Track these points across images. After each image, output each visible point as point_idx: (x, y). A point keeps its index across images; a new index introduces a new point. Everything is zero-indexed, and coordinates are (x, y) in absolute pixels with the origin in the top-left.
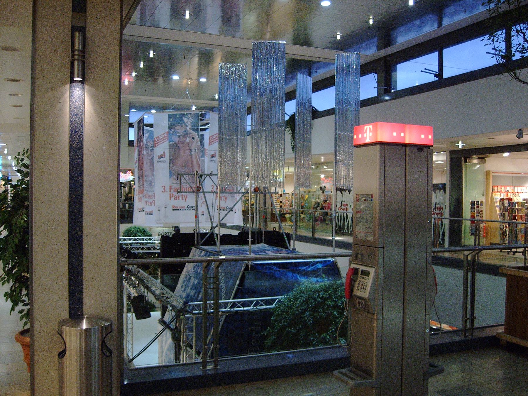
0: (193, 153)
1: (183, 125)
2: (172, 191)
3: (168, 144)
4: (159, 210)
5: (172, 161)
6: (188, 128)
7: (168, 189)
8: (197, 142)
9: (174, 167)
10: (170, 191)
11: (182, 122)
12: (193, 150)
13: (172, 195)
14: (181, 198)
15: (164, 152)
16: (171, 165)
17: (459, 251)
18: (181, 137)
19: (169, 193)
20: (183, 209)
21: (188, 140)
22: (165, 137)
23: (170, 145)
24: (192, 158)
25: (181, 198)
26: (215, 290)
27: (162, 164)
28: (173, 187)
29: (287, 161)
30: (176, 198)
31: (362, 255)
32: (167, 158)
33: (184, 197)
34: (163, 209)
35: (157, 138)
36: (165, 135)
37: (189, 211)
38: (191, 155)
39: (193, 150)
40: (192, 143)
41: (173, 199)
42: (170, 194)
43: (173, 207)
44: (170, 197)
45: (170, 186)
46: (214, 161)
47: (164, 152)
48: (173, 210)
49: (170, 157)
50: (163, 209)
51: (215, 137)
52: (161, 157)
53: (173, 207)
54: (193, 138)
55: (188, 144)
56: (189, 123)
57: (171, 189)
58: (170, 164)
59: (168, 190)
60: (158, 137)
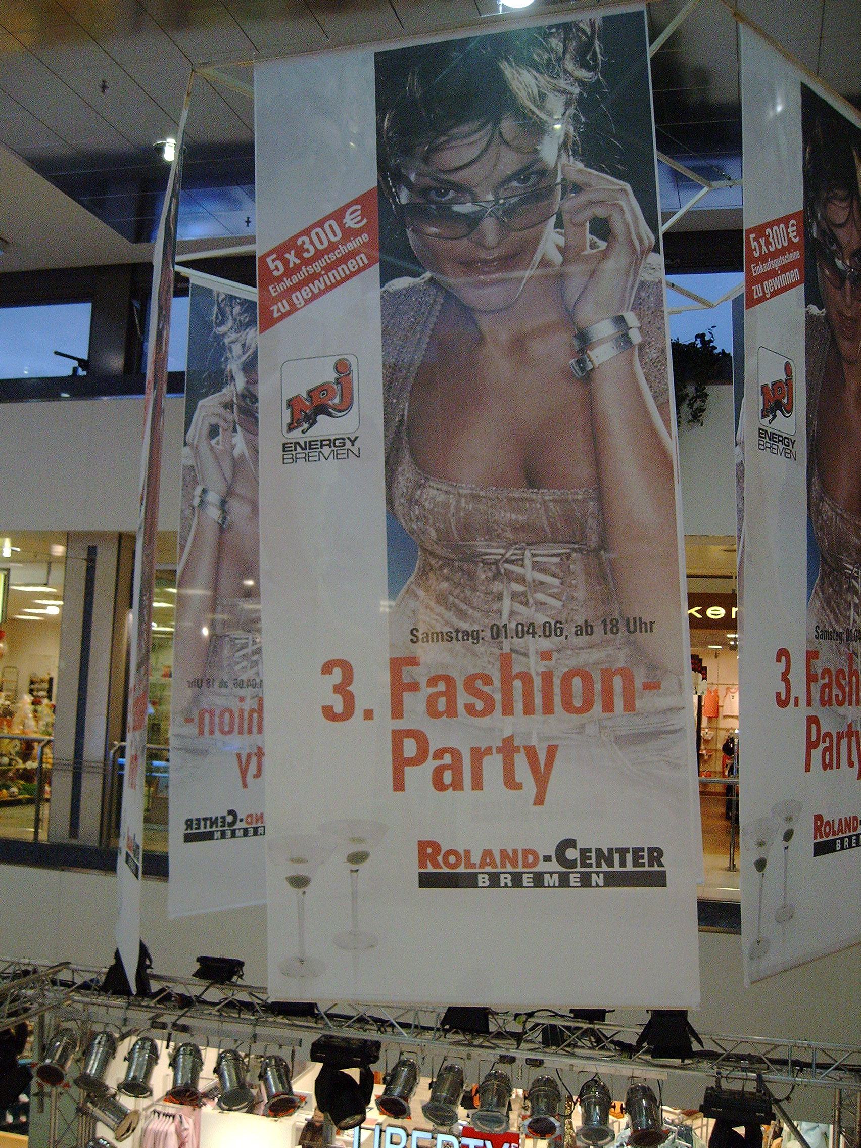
0: (602, 354)
1: (508, 126)
2: (415, 703)
4: (299, 882)
5: (413, 440)
6: (549, 152)
7: (373, 687)
10: (397, 712)
12: (604, 329)
13: (410, 748)
14: (493, 766)
15: (342, 368)
16: (406, 473)
17: (308, 1027)
19: (385, 723)
20: (513, 873)
22: (349, 235)
24: (590, 403)
25: (493, 766)
27: (326, 470)
28: (420, 674)
29: (195, 442)
32: (365, 418)
35: (280, 252)
36: (350, 221)
37: (575, 894)
38: (585, 376)
39: (604, 329)
41: (419, 777)
42: (398, 737)
43: (427, 849)
44: (400, 764)
45: (397, 665)
46: (340, 446)
47: (342, 368)
48: (426, 881)
50: (329, 874)
52: (310, 408)
53: (427, 849)
56: (556, 103)
57: (400, 688)
59: (383, 710)
60: (290, 245)
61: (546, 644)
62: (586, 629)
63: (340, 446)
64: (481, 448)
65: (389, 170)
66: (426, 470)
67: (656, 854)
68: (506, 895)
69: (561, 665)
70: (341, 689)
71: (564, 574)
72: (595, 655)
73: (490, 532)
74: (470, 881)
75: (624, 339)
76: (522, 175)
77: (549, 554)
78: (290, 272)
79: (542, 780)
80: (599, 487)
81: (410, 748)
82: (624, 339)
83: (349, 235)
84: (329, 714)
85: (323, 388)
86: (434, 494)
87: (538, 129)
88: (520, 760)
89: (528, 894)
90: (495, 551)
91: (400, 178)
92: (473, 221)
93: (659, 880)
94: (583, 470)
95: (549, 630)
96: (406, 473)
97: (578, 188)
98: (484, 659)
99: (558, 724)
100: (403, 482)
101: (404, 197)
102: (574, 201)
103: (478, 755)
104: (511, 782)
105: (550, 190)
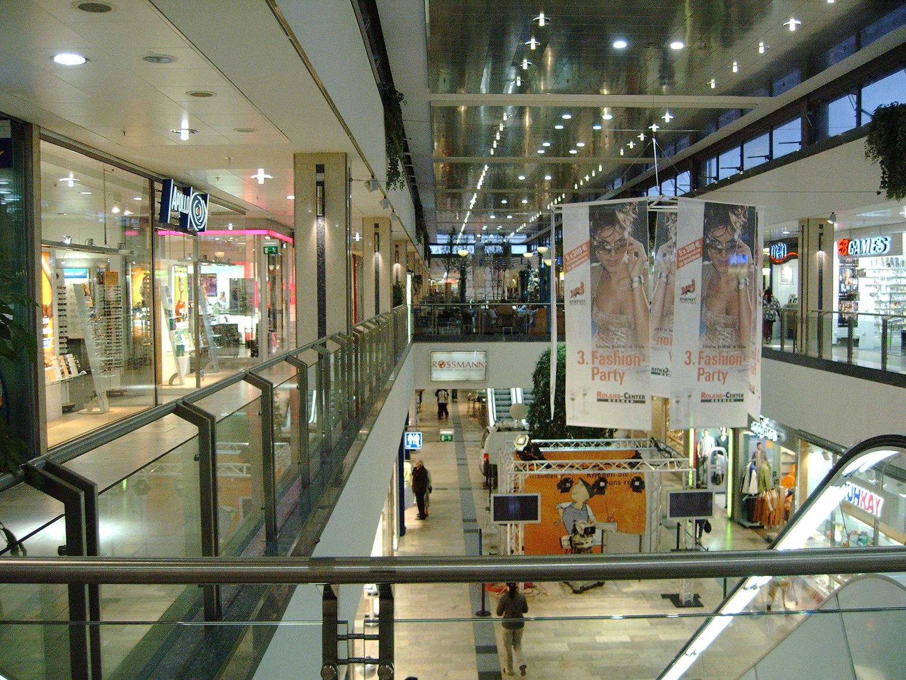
1: (617, 227)
2: (703, 361)
3: (701, 265)
6: (626, 235)
8: (643, 263)
9: (601, 315)
11: (726, 222)
12: (636, 279)
15: (582, 284)
16: (595, 309)
18: (613, 252)
19: (590, 365)
21: (626, 257)
22: (697, 248)
23: (592, 269)
24: (633, 295)
26: (342, 630)
27: (689, 305)
30: (604, 377)
31: (512, 674)
32: (697, 294)
33: (618, 378)
34: (684, 399)
37: (627, 404)
38: (632, 289)
40: (635, 264)
43: (703, 394)
46: (692, 300)
48: (702, 401)
49: (592, 294)
51: (692, 247)
52: (686, 290)
53: (703, 394)
54: (636, 254)
55: (627, 266)
56: (628, 222)
58: (702, 305)
59: (590, 362)
60: (571, 253)
61: (727, 350)
62: (631, 347)
63: (692, 300)
64: (610, 305)
65: (592, 237)
66: (708, 309)
67: (643, 397)
68: (614, 404)
69: (626, 354)
70: (582, 357)
71: (626, 334)
72: (632, 353)
73: (611, 324)
74: (710, 401)
75: (640, 282)
76: (620, 240)
77: (624, 330)
78: (684, 255)
79: (621, 379)
80: (634, 316)
81: (596, 371)
82: (640, 282)
83: (697, 248)
84: (579, 362)
85: (578, 289)
86: (709, 314)
87: (623, 228)
88: (618, 375)
89: (618, 404)
90: (613, 329)
91: (594, 239)
92: (610, 251)
93: (644, 402)
94: (736, 311)
95: (624, 347)
96: (595, 309)
97: (632, 244)
98: (610, 352)
99: (625, 367)
100: (594, 311)
101: (708, 242)
102: (631, 247)
103: (609, 373)
104: (719, 379)
105: (625, 245)
